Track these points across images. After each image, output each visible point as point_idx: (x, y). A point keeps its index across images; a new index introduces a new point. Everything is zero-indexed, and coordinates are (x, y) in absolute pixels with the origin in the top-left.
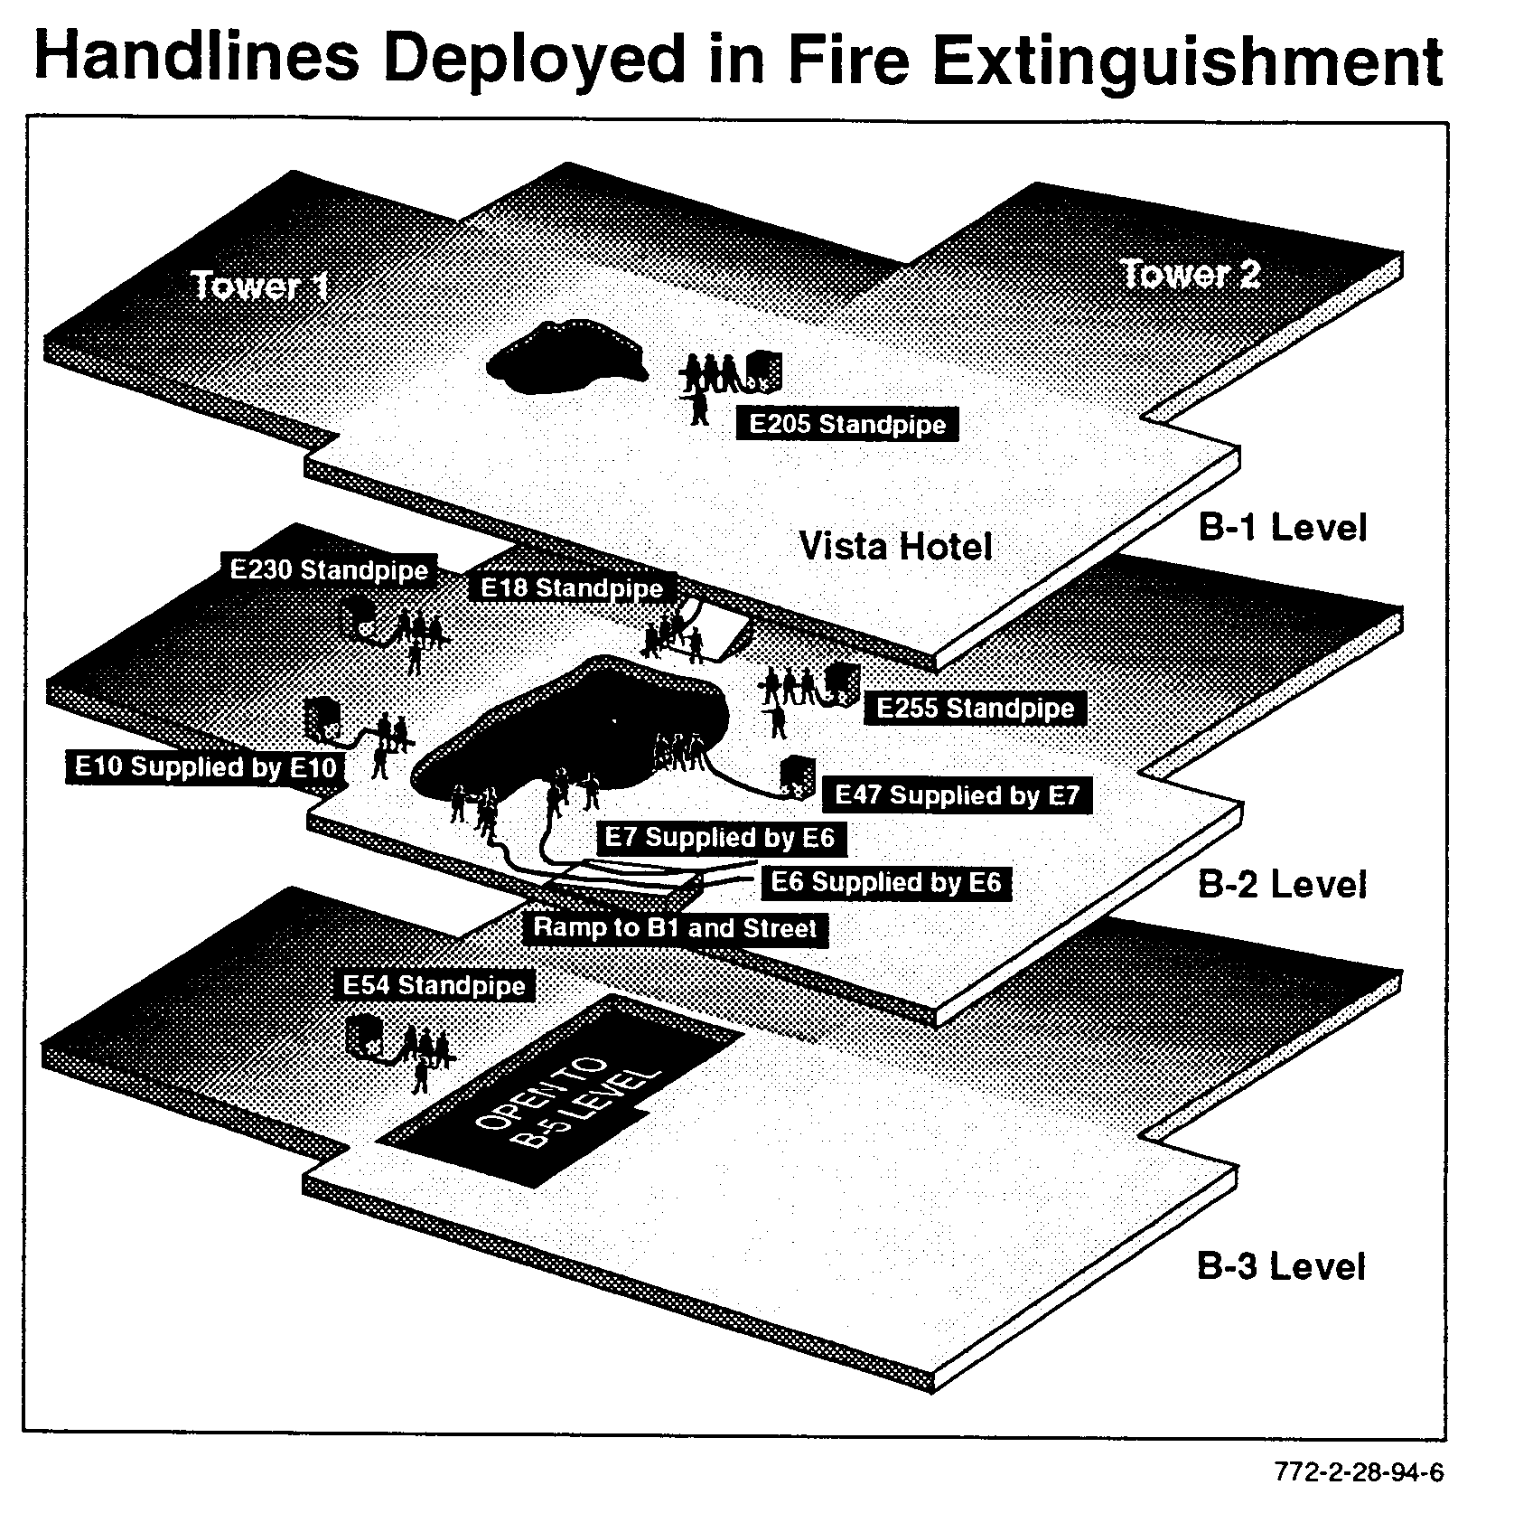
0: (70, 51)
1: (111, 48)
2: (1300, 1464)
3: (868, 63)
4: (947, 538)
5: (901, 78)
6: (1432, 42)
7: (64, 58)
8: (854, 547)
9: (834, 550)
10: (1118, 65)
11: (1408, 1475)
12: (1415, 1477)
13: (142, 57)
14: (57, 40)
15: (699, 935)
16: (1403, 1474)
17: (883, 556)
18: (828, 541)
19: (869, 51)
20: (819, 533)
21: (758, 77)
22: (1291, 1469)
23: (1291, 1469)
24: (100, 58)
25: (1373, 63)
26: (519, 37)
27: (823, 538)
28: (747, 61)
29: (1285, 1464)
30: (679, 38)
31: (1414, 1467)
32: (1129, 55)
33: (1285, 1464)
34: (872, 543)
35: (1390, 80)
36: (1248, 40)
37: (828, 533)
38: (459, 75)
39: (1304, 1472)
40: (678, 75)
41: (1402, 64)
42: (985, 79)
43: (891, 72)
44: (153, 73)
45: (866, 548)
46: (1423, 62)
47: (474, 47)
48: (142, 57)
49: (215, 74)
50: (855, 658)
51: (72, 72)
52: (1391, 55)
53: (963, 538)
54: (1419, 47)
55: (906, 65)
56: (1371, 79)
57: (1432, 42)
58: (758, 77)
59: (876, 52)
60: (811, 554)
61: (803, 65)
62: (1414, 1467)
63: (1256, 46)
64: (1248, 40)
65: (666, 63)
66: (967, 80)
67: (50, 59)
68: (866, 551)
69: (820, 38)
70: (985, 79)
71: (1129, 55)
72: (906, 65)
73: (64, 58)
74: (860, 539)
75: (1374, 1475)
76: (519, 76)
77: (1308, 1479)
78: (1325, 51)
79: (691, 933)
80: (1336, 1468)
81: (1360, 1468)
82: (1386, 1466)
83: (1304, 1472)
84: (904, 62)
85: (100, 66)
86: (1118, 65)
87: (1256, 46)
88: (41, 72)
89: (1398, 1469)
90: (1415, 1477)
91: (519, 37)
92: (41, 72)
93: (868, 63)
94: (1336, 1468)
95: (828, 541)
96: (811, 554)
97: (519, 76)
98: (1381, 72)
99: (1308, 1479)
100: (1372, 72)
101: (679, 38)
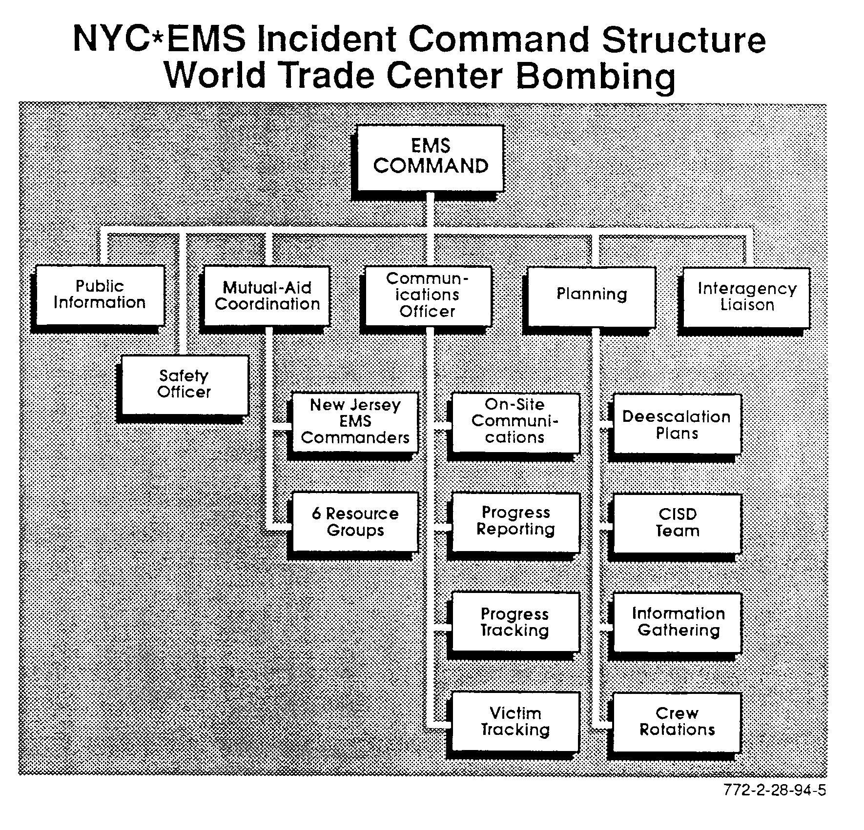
2: (739, 785)
3: (744, 42)
6: (391, 29)
10: (610, 79)
13: (556, 40)
19: (650, 35)
22: (733, 788)
24: (321, 78)
28: (721, 614)
30: (586, 29)
31: (808, 787)
32: (604, 85)
33: (730, 785)
36: (603, 65)
39: (742, 789)
40: (585, 48)
46: (385, 40)
48: (556, 40)
49: (626, 86)
57: (391, 29)
62: (808, 787)
63: (607, 69)
64: (603, 65)
65: (579, 42)
66: (186, 49)
69: (186, 27)
71: (604, 85)
73: (292, 67)
77: (743, 794)
80: (761, 787)
81: (776, 787)
83: (742, 789)
84: (371, 76)
86: (610, 79)
87: (607, 69)
89: (799, 788)
90: (809, 793)
93: (744, 42)
99: (743, 794)
101: (586, 29)
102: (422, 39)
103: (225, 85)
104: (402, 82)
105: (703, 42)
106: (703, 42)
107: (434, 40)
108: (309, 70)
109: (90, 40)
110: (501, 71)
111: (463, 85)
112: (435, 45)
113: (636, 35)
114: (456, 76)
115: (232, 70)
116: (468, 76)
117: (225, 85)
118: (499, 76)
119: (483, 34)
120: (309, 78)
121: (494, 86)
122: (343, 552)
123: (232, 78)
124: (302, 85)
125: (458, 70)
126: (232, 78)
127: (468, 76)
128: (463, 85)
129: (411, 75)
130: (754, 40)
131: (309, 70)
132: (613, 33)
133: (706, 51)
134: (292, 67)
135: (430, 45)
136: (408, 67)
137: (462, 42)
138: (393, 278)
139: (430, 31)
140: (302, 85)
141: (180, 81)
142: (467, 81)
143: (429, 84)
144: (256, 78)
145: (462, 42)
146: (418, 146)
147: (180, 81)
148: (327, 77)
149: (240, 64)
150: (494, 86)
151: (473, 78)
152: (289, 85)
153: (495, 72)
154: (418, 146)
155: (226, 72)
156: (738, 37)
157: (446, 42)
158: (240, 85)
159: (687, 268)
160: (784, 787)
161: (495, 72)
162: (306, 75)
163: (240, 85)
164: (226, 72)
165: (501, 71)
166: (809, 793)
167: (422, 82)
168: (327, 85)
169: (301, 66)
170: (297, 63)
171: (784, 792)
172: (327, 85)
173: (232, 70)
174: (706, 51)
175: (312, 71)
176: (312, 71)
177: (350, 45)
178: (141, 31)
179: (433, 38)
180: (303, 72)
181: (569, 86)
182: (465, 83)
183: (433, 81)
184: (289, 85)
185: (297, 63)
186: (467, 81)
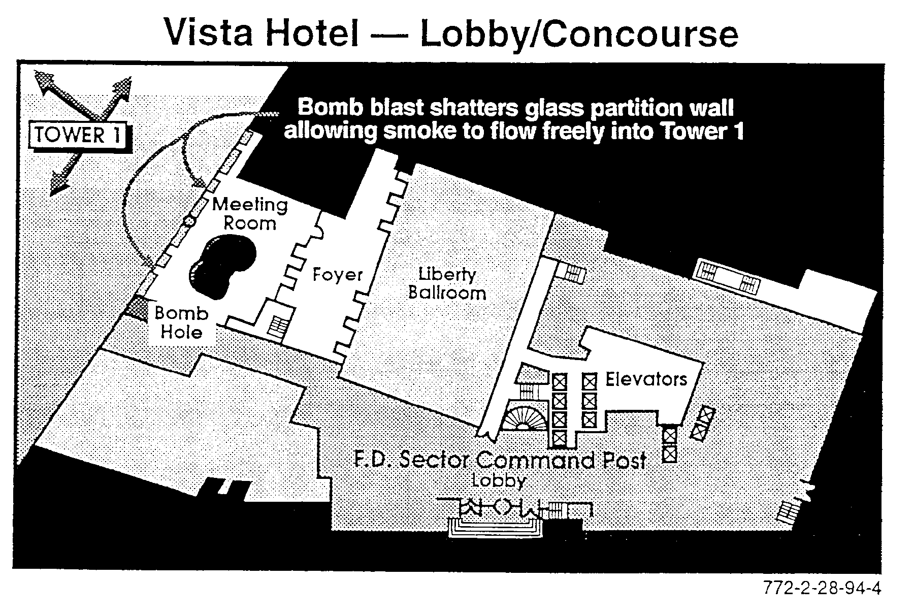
0: (285, 32)
4: (313, 26)
5: (735, 43)
7: (282, 35)
8: (219, 33)
9: (198, 36)
13: (671, 38)
14: (278, 25)
15: (294, 136)
17: (249, 42)
18: (192, 28)
19: (695, 29)
20: (183, 21)
21: (275, 228)
22: (775, 586)
23: (775, 586)
27: (187, 24)
29: (771, 582)
34: (238, 29)
37: (192, 19)
38: (345, 42)
39: (784, 588)
40: (249, 42)
44: (665, 29)
45: (232, 35)
51: (286, 43)
53: (329, 25)
54: (218, 24)
56: (345, 42)
58: (275, 228)
59: (699, 29)
60: (175, 41)
61: (274, 35)
63: (495, 27)
64: (469, 22)
67: (274, 35)
68: (231, 38)
74: (226, 26)
75: (850, 585)
77: (786, 593)
79: (286, 135)
80: (806, 585)
81: (823, 585)
83: (784, 588)
87: (495, 27)
88: (270, 43)
89: (850, 585)
92: (270, 43)
95: (192, 28)
96: (175, 41)
99: (786, 593)
104: (557, 40)
111: (322, 43)
113: (230, 27)
116: (326, 33)
121: (355, 43)
122: (129, 569)
125: (222, 27)
128: (322, 43)
130: (336, 32)
132: (707, 32)
133: (325, 44)
135: (563, 40)
136: (563, 26)
142: (327, 38)
146: (89, 135)
150: (355, 43)
151: (332, 36)
154: (89, 135)
156: (688, 31)
157: (647, 37)
158: (609, 44)
159: (657, 421)
160: (833, 585)
166: (863, 591)
171: (834, 590)
174: (325, 44)
178: (558, 26)
179: (566, 33)
181: (597, 44)
182: (324, 40)
186: (327, 38)
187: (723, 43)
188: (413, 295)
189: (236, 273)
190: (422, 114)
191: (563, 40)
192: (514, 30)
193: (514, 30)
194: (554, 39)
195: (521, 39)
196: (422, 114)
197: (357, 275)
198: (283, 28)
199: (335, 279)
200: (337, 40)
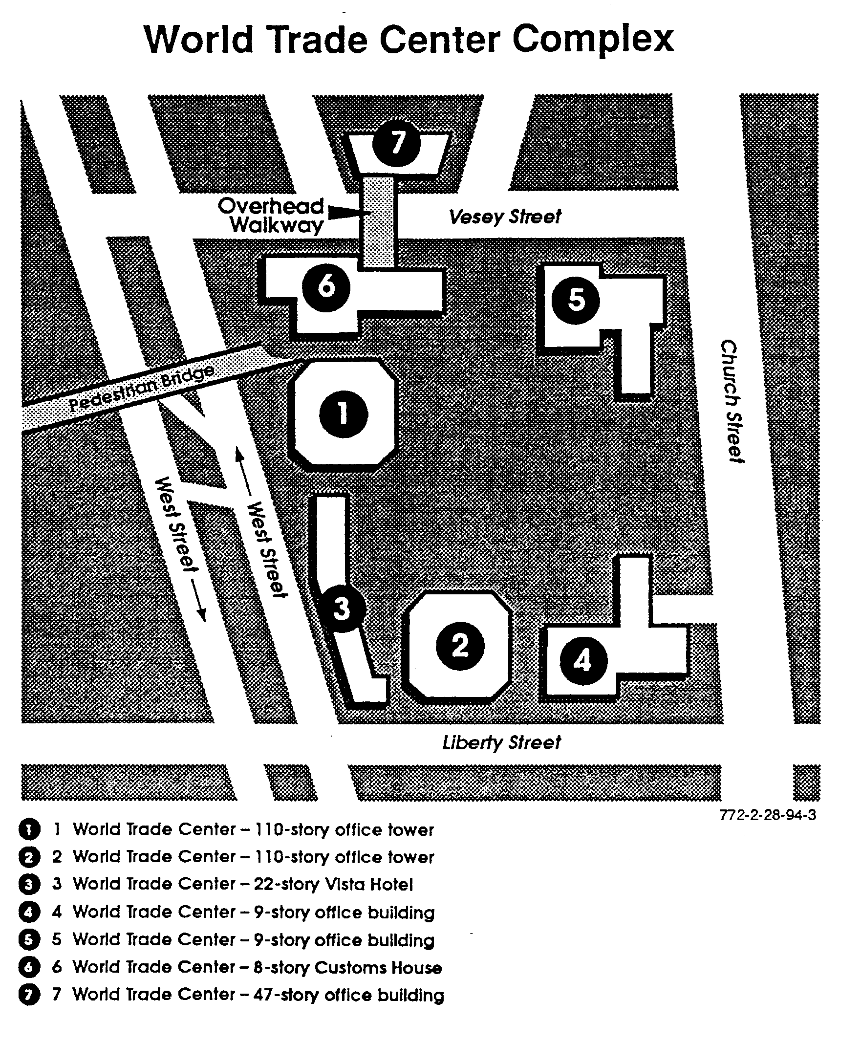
1: (318, 36)
2: (734, 811)
5: (364, 49)
11: (796, 816)
12: (800, 817)
16: (792, 816)
24: (358, 43)
25: (482, 41)
26: (626, 26)
30: (250, 28)
33: (726, 811)
35: (433, 50)
39: (737, 815)
41: (440, 41)
42: (659, 48)
43: (642, 45)
47: (432, 34)
50: (148, 369)
52: (434, 36)
54: (451, 31)
55: (366, 43)
56: (482, 48)
70: (659, 48)
72: (366, 43)
73: (282, 31)
76: (626, 48)
77: (738, 819)
78: (587, 32)
80: (755, 813)
81: (768, 812)
82: (287, 853)
84: (364, 41)
85: (312, 46)
89: (790, 813)
90: (800, 817)
91: (626, 26)
94: (741, 812)
97: (626, 48)
98: (487, 45)
99: (738, 819)
100: (424, 45)
101: (250, 28)
102: (527, 39)
103: (209, 50)
104: (397, 46)
105: (458, 42)
106: (458, 42)
107: (539, 40)
108: (299, 35)
109: (169, 42)
110: (498, 34)
111: (459, 50)
112: (539, 46)
114: (453, 40)
115: (217, 35)
116: (464, 40)
117: (209, 50)
118: (496, 39)
119: (590, 34)
120: (299, 43)
121: (492, 49)
123: (217, 43)
124: (292, 50)
126: (217, 43)
127: (464, 40)
128: (459, 50)
129: (405, 39)
131: (299, 35)
134: (282, 31)
135: (535, 44)
136: (402, 31)
137: (568, 42)
138: (227, 205)
139: (535, 30)
140: (292, 50)
141: (162, 45)
143: (424, 49)
144: (242, 42)
145: (568, 42)
147: (162, 45)
148: (318, 41)
149: (225, 28)
151: (470, 42)
152: (278, 50)
153: (493, 36)
155: (211, 36)
157: (551, 41)
158: (225, 50)
161: (493, 36)
162: (297, 40)
163: (225, 50)
164: (211, 36)
165: (498, 34)
167: (416, 47)
168: (318, 50)
169: (291, 30)
170: (286, 27)
171: (776, 817)
172: (318, 50)
173: (217, 35)
175: (302, 35)
176: (302, 35)
177: (356, 47)
179: (538, 38)
180: (293, 37)
181: (568, 49)
183: (428, 45)
184: (278, 50)
185: (286, 27)
187: (412, 48)
188: (167, 383)
189: (296, 448)
190: (340, 404)
191: (402, 46)
192: (496, 214)
193: (496, 214)
194: (525, 44)
195: (154, 42)
196: (340, 404)
197: (230, 883)
198: (273, 32)
199: (494, 221)
200: (356, 47)
